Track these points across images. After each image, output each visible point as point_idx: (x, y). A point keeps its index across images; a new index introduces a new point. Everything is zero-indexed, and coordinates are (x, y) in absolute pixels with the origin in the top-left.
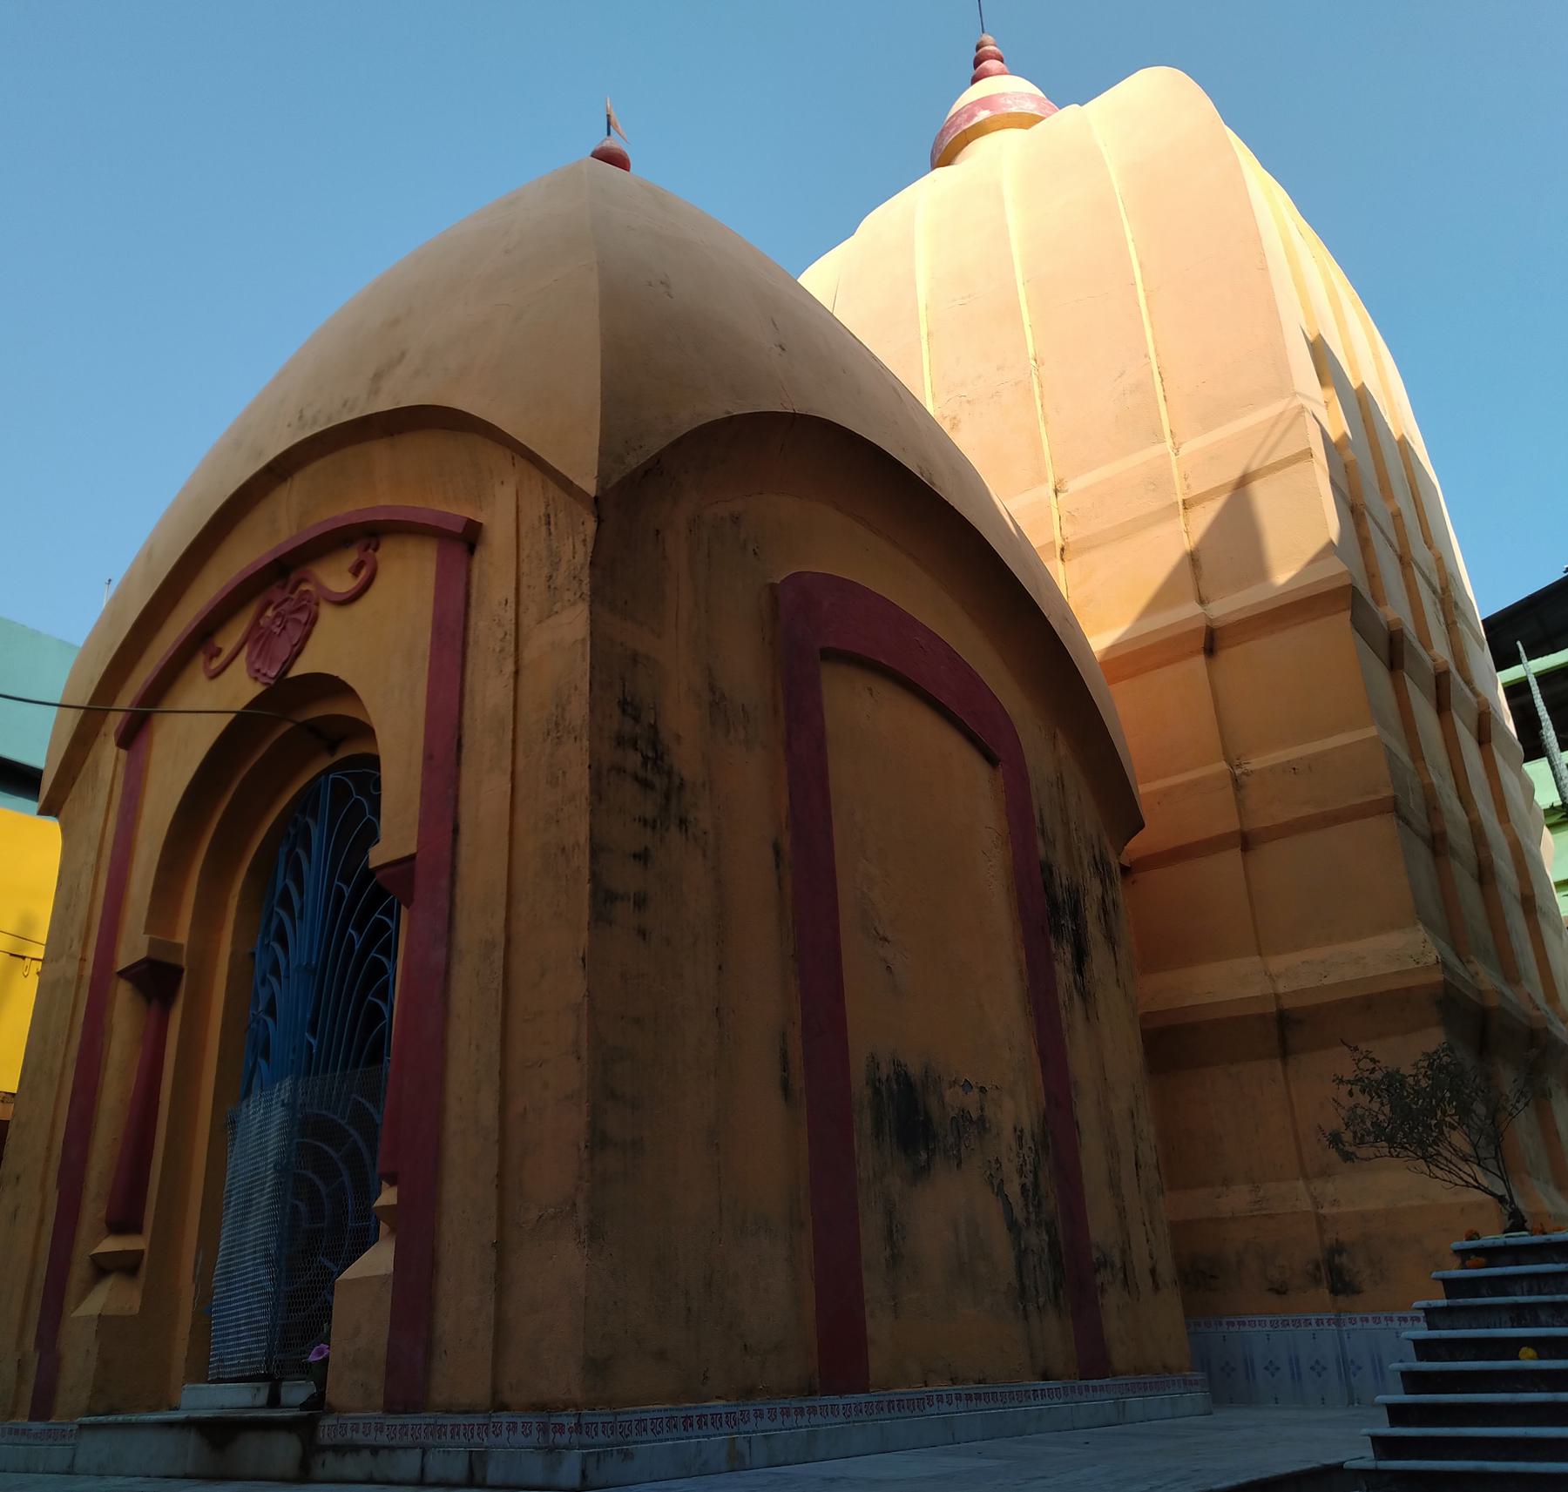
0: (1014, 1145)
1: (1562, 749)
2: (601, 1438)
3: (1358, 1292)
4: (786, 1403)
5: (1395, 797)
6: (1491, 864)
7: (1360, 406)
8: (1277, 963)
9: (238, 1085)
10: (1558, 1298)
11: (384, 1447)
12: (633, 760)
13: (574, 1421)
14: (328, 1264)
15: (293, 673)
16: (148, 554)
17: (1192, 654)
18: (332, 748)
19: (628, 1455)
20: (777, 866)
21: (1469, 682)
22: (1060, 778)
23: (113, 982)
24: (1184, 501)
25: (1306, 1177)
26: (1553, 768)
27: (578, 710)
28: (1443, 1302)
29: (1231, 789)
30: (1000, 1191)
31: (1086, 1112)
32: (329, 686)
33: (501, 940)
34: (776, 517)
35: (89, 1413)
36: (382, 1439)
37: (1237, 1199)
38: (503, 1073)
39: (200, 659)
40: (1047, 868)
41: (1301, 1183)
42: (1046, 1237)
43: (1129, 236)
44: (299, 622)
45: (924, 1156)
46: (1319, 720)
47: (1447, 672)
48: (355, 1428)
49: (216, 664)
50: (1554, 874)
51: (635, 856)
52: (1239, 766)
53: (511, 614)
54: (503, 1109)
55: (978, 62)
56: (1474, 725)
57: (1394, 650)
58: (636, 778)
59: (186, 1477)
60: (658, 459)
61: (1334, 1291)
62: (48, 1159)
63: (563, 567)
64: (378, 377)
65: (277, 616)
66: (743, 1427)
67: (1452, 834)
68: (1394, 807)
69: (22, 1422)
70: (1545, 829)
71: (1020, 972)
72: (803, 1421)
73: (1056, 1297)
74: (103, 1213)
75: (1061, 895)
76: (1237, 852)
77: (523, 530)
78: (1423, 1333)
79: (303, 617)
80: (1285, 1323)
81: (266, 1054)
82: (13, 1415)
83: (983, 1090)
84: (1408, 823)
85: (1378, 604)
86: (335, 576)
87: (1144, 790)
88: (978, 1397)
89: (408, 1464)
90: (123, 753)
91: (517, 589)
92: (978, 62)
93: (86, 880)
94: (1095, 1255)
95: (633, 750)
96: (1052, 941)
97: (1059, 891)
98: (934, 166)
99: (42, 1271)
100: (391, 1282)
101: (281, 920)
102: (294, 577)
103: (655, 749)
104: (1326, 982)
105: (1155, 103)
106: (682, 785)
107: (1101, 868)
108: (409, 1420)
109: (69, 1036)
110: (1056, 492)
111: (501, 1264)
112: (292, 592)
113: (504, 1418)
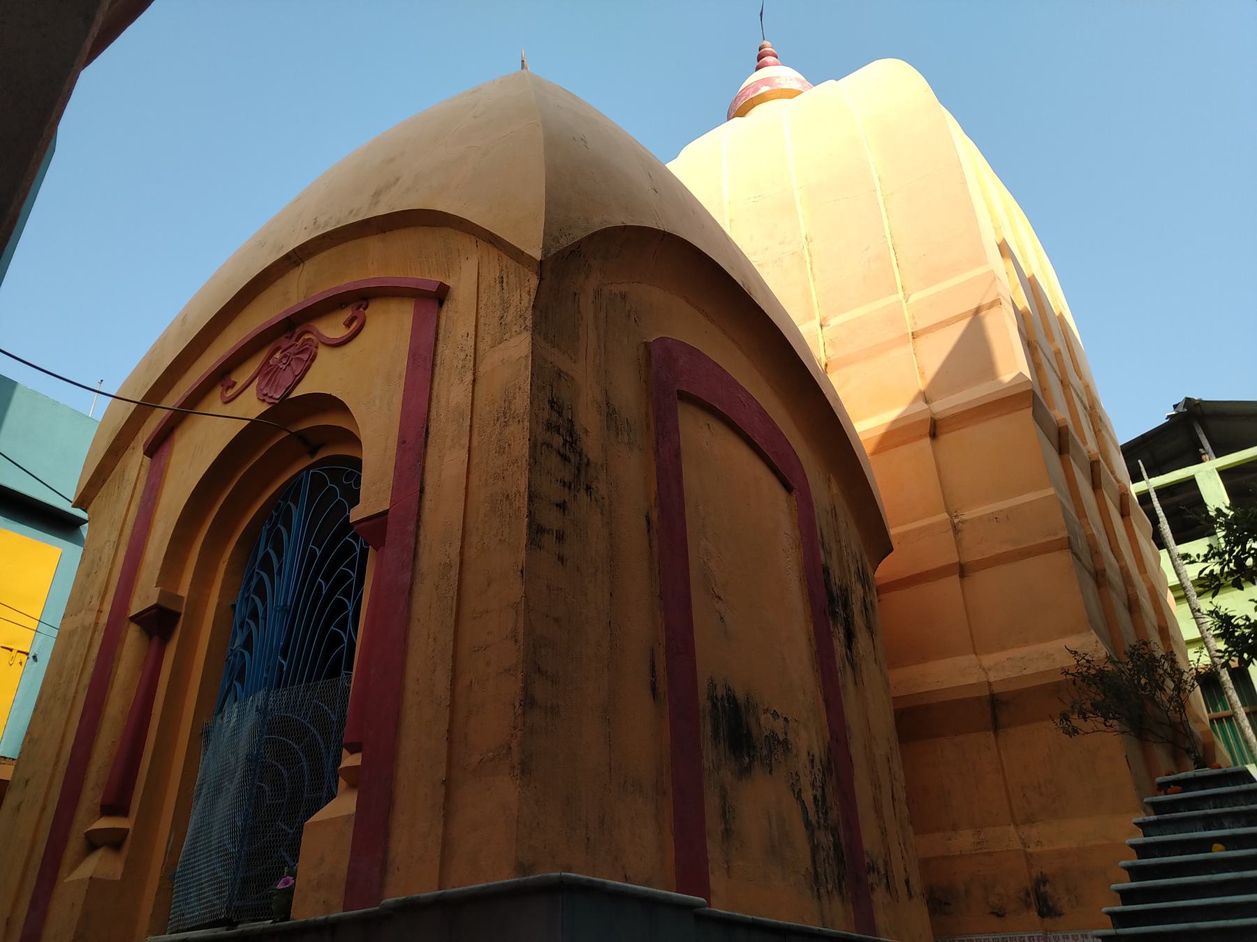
0: (808, 765)
1: (1177, 544)
3: (1060, 915)
6: (1137, 599)
7: (1032, 287)
8: (988, 660)
9: (213, 705)
10: (1236, 809)
12: (557, 441)
16: (183, 319)
17: (921, 437)
18: (313, 452)
21: (1113, 473)
25: (1017, 825)
27: (522, 402)
34: (646, 305)
37: (964, 841)
38: (454, 657)
39: (218, 390)
40: (826, 570)
41: (1012, 828)
45: (747, 760)
46: (1009, 486)
47: (1098, 462)
49: (230, 393)
54: (453, 682)
55: (760, 58)
56: (1118, 503)
57: (1062, 441)
60: (579, 244)
61: (1042, 915)
63: (512, 310)
64: (377, 194)
65: (285, 356)
67: (1109, 573)
68: (1068, 545)
73: (840, 887)
74: (99, 800)
75: (835, 591)
76: (956, 577)
77: (482, 290)
78: (1140, 839)
79: (305, 357)
84: (1079, 559)
86: (333, 328)
87: (893, 532)
90: (147, 459)
91: (476, 326)
92: (760, 58)
93: (108, 553)
94: (867, 860)
97: (834, 588)
99: (41, 849)
100: (353, 819)
101: (262, 579)
102: (298, 331)
103: (571, 436)
104: (1025, 672)
106: (588, 464)
110: (821, 326)
111: (448, 797)
112: (297, 340)
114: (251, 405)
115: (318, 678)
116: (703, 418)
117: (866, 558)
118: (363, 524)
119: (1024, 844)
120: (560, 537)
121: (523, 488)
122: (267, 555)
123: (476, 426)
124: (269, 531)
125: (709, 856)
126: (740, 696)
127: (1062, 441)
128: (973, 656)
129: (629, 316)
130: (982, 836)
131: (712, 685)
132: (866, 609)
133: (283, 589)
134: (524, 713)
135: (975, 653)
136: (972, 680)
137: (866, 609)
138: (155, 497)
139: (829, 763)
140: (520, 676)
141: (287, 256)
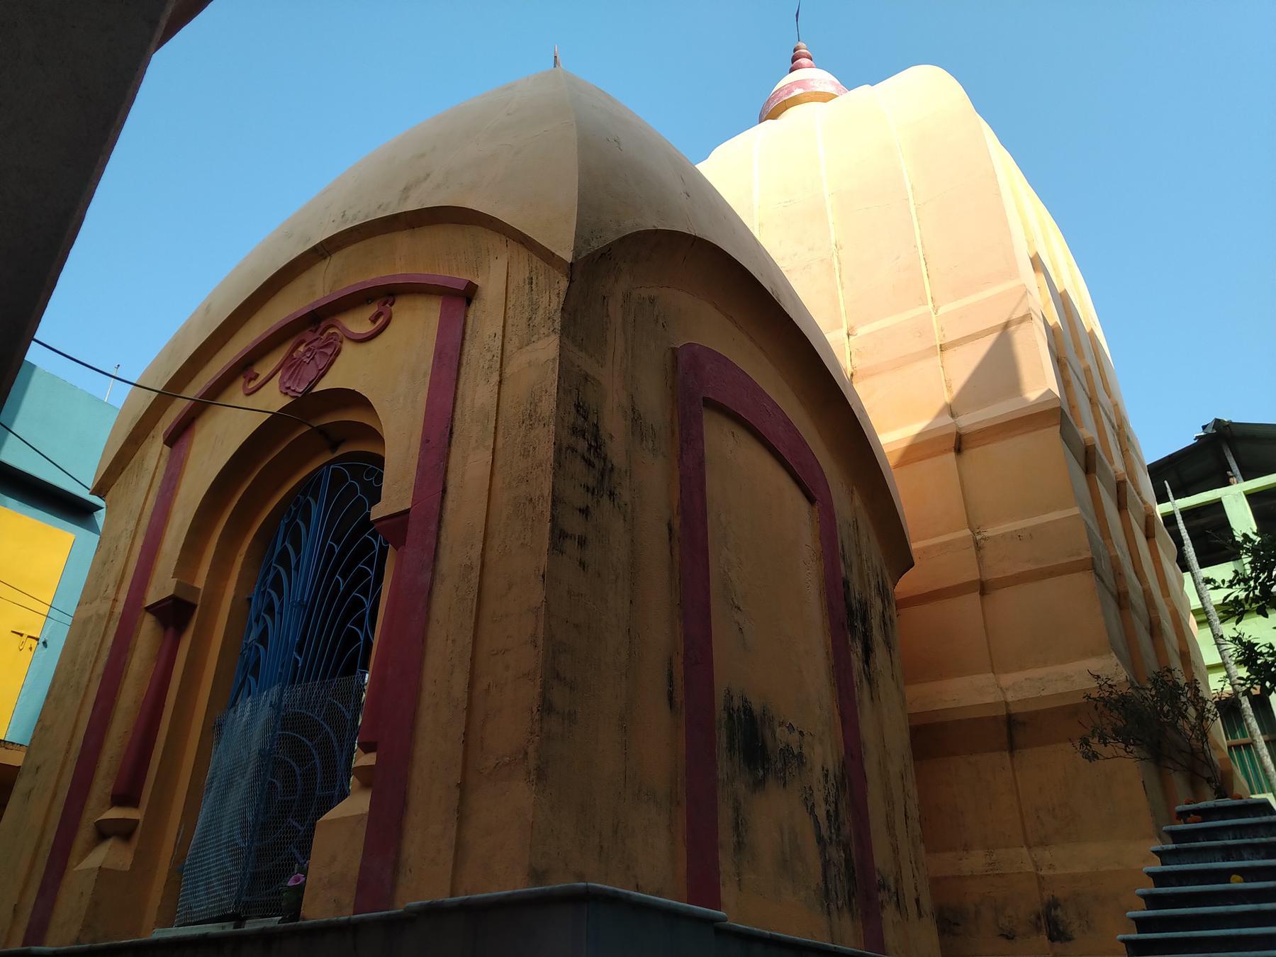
0: (822, 779)
3: (1070, 939)
8: (1007, 679)
9: (226, 698)
10: (1256, 840)
12: (582, 445)
14: (296, 824)
15: (315, 390)
16: (207, 309)
17: (945, 451)
21: (1139, 494)
25: (1029, 847)
27: (548, 406)
28: (1172, 846)
30: (811, 811)
31: (871, 767)
33: (478, 564)
34: (676, 308)
37: (975, 861)
40: (846, 583)
41: (1025, 850)
47: (1124, 482)
49: (253, 385)
53: (498, 343)
54: (471, 685)
55: (794, 59)
56: (1143, 522)
57: (1089, 460)
58: (583, 457)
60: (610, 248)
61: (1052, 938)
63: (541, 311)
64: (407, 189)
65: (309, 350)
68: (1091, 566)
74: (109, 790)
75: (855, 605)
78: (1157, 867)
79: (329, 351)
86: (358, 323)
87: (914, 546)
90: (167, 449)
91: (504, 327)
92: (794, 59)
93: (124, 543)
97: (853, 602)
99: (51, 837)
100: (366, 818)
102: (323, 325)
104: (1043, 693)
106: (612, 469)
109: (97, 658)
111: (462, 800)
114: (273, 399)
115: (333, 676)
116: (728, 426)
119: (1037, 868)
120: (582, 542)
122: (285, 550)
123: (501, 428)
124: (288, 525)
127: (1089, 460)
129: (657, 321)
131: (729, 696)
132: (885, 624)
133: (300, 584)
136: (989, 700)
137: (885, 624)
139: (843, 779)
140: (538, 681)
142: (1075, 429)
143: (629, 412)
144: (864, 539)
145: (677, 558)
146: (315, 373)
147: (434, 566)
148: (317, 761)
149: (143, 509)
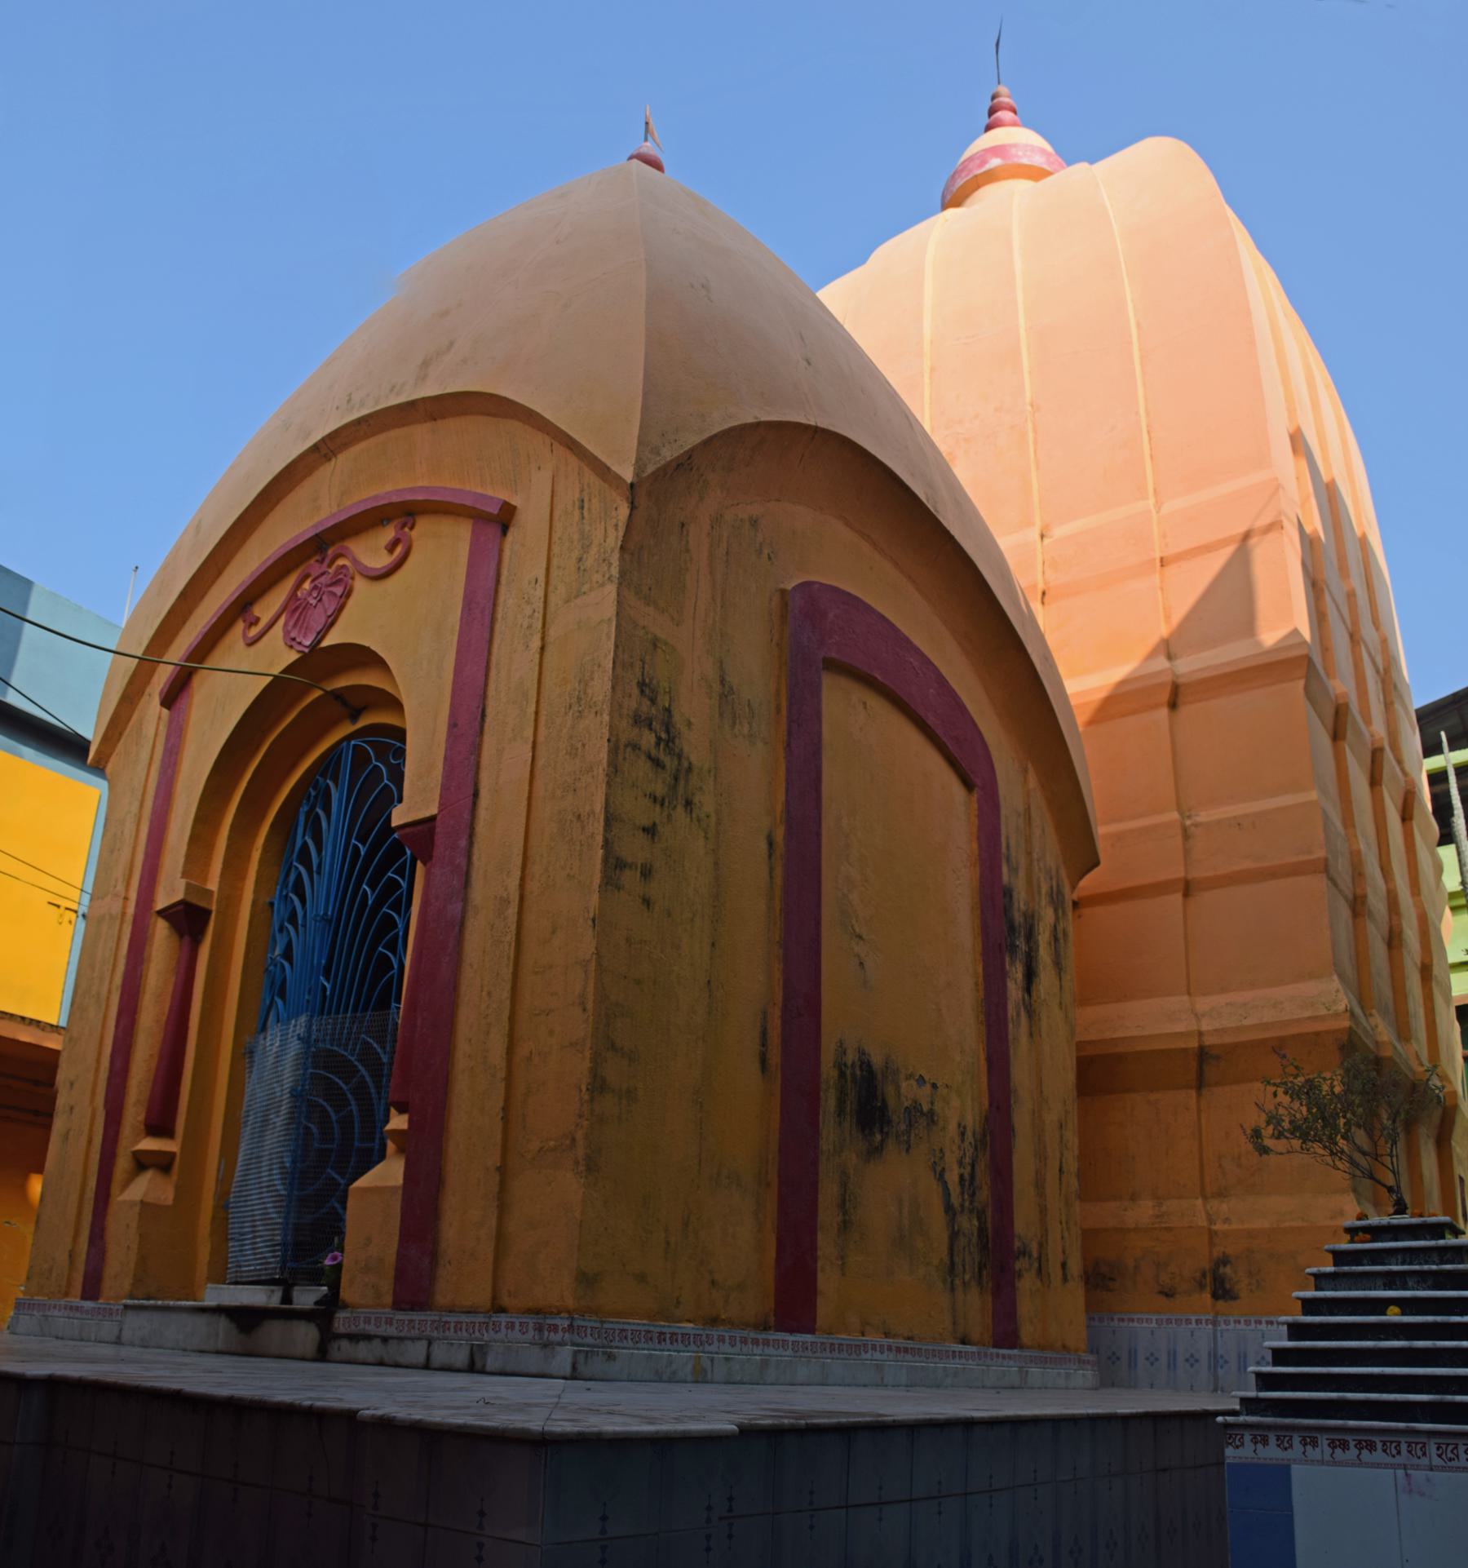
0: (957, 1140)
2: (589, 1340)
3: (1235, 1298)
4: (745, 1333)
5: (1326, 860)
6: (1401, 932)
7: (1330, 497)
8: (1203, 1004)
9: (255, 1022)
11: (392, 1338)
12: (648, 739)
13: (566, 1323)
15: (325, 644)
16: (197, 527)
17: (1156, 706)
18: (354, 716)
19: (611, 1357)
20: (770, 856)
21: (1400, 762)
22: (1028, 810)
23: (158, 925)
24: (1162, 559)
25: (1205, 1198)
26: (1459, 854)
27: (601, 687)
29: (1179, 838)
30: (941, 1177)
31: (1021, 1119)
32: (361, 657)
35: (132, 1297)
36: (391, 1331)
37: (1142, 1212)
39: (240, 626)
40: (1008, 893)
41: (1199, 1202)
42: (976, 1223)
43: (1129, 297)
44: (334, 594)
45: (878, 1137)
47: (1382, 750)
48: (367, 1321)
49: (254, 632)
50: (1454, 955)
51: (644, 829)
52: (1189, 817)
53: (540, 592)
55: (992, 111)
56: (1400, 802)
58: (650, 757)
59: (218, 1352)
60: (689, 454)
61: (1215, 1296)
62: (97, 1070)
63: (594, 550)
64: (426, 364)
65: (315, 588)
66: (707, 1348)
68: (1324, 868)
69: (76, 1301)
70: (1447, 911)
71: (976, 984)
72: (758, 1350)
73: (980, 1276)
74: (142, 1117)
75: (1018, 918)
76: (1179, 897)
77: (557, 513)
79: (338, 590)
80: (1169, 1321)
81: (282, 994)
82: (66, 1294)
83: (934, 1086)
84: (1335, 884)
85: (1328, 675)
86: (371, 551)
87: (1101, 831)
88: (906, 1350)
89: (417, 1352)
90: (165, 711)
91: (548, 569)
92: (992, 111)
93: (129, 828)
94: (1017, 1244)
95: (649, 732)
96: (1007, 959)
98: (945, 206)
100: (400, 1192)
101: (299, 875)
103: (668, 731)
104: (1246, 1022)
105: (1157, 176)
106: (690, 769)
107: (1056, 900)
108: (416, 1316)
110: (1042, 536)
112: (330, 566)
113: (503, 1319)
114: (276, 655)
115: (365, 1009)
116: (859, 693)
117: (1063, 873)
118: (408, 830)
119: (1211, 1221)
120: (647, 873)
121: (599, 807)
122: (305, 845)
123: (543, 713)
124: (308, 814)
125: (819, 1253)
126: (877, 1060)
127: (1339, 725)
128: (1186, 998)
129: (760, 552)
130: (1164, 1208)
131: (842, 1050)
132: (1056, 939)
133: (321, 895)
134: (592, 1100)
135: (1189, 994)
136: (1180, 1028)
137: (1056, 939)
138: (175, 764)
139: (985, 1135)
140: (588, 1054)
141: (315, 448)
142: (1322, 687)
143: (717, 687)
144: (1037, 832)
145: (779, 880)
146: (323, 620)
147: (466, 894)
148: (354, 1108)
149: (145, 786)
